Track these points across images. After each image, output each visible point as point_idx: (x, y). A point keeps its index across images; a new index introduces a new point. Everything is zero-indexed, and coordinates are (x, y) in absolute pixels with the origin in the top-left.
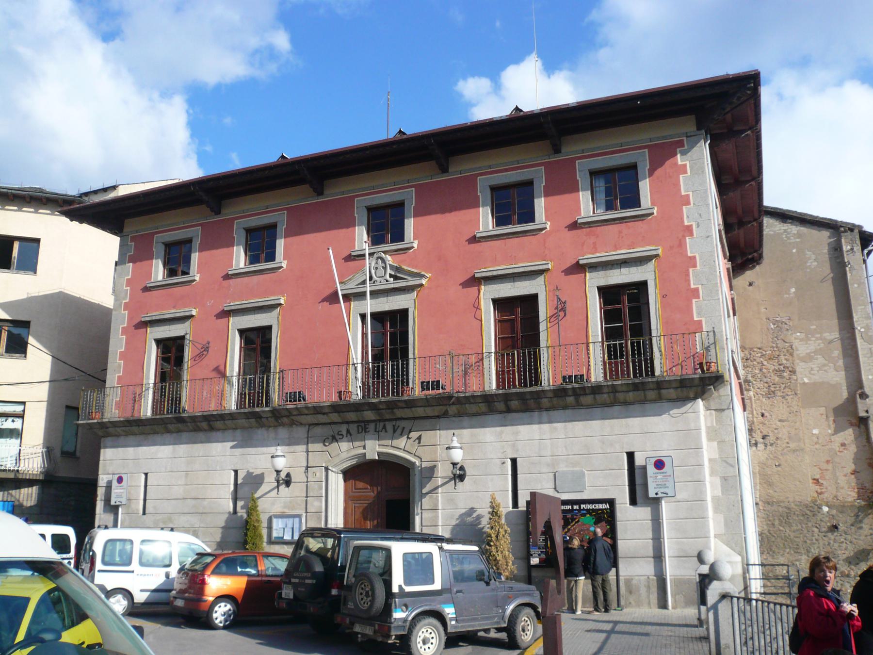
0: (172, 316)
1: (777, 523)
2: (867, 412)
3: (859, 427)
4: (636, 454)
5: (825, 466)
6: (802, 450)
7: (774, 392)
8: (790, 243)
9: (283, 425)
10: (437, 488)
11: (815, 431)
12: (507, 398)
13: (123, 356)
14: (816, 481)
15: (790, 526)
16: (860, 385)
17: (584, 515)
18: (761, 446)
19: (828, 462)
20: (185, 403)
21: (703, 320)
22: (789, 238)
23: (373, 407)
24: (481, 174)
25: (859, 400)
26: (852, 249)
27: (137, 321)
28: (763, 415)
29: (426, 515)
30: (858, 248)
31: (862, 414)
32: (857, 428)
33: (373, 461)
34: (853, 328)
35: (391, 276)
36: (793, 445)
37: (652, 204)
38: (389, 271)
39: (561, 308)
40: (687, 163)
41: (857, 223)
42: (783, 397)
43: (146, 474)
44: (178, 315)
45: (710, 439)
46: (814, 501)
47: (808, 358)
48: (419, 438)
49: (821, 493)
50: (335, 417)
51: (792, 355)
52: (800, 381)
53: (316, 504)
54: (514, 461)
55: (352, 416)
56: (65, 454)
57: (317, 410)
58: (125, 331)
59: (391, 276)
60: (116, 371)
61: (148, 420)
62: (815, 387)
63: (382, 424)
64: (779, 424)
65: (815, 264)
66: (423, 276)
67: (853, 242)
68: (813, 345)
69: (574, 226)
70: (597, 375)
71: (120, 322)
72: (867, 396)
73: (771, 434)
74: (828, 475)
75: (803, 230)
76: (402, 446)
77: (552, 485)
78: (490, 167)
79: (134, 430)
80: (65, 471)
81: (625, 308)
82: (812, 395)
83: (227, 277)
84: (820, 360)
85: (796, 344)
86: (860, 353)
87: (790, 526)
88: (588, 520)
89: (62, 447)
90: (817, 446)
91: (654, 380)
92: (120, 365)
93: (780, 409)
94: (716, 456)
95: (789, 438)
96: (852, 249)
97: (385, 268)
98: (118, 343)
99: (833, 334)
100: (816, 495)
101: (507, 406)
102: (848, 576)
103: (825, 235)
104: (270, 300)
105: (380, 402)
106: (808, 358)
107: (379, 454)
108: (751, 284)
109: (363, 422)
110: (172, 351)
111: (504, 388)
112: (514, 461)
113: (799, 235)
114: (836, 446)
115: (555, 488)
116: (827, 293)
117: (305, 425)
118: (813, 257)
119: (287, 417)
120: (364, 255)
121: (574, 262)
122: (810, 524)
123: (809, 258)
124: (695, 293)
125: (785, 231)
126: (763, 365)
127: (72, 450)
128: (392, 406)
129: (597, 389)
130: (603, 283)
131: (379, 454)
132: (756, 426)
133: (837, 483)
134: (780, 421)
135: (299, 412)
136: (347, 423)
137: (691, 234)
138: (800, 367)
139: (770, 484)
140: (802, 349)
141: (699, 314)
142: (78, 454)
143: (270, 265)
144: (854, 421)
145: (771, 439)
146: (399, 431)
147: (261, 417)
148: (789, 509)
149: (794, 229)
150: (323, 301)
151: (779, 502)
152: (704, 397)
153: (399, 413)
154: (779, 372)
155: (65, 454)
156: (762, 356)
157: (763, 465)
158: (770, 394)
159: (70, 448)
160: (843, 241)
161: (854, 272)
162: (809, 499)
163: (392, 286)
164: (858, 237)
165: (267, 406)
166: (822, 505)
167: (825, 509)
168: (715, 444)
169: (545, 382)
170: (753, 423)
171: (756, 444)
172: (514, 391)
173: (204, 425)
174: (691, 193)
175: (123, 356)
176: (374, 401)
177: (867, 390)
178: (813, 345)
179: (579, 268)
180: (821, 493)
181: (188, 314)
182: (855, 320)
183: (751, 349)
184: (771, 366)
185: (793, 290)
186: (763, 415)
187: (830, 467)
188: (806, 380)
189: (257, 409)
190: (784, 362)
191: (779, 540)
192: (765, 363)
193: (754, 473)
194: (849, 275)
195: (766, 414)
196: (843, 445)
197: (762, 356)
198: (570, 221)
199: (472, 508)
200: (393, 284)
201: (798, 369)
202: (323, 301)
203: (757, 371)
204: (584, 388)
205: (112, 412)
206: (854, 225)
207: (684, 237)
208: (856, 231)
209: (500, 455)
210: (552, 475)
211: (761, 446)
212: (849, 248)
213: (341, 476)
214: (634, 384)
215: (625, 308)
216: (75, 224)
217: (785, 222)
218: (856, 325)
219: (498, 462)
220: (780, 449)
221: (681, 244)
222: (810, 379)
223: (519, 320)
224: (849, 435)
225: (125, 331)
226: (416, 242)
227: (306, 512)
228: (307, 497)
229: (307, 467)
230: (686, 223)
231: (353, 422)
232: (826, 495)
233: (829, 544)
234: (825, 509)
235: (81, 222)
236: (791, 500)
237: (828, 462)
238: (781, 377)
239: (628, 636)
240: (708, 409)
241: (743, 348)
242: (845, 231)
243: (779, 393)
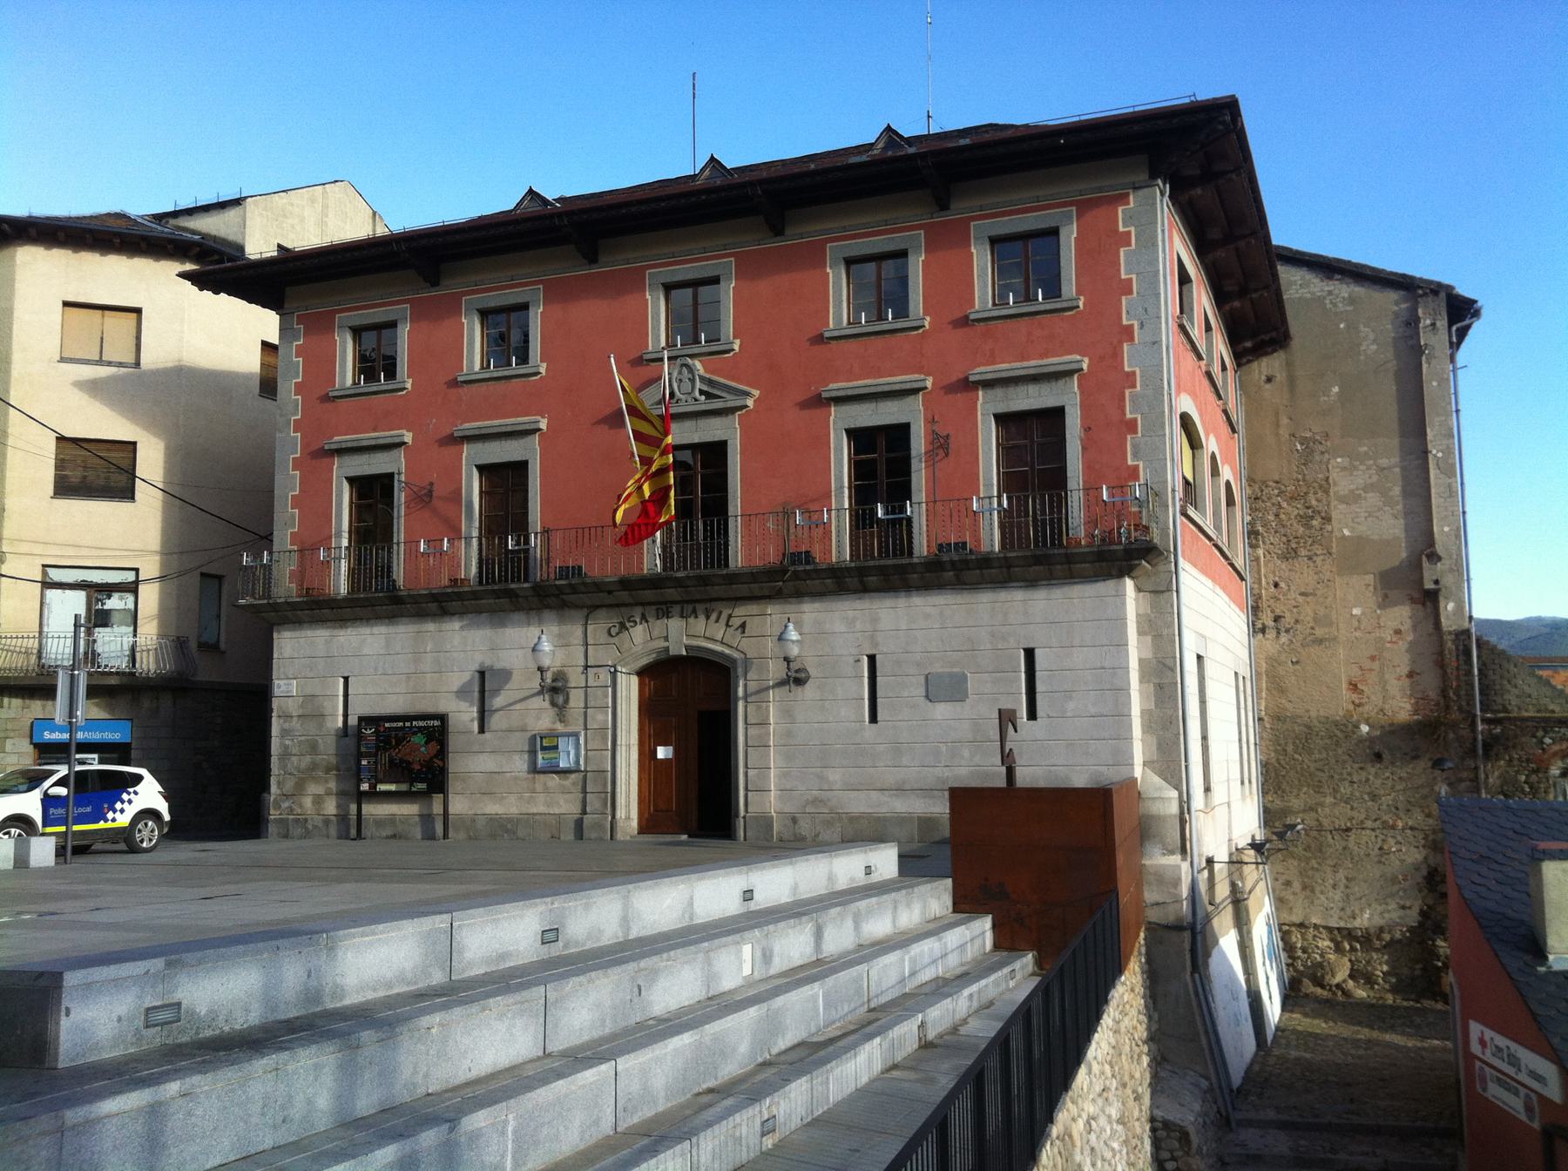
0: (373, 443)
1: (1290, 748)
2: (1437, 582)
3: (1424, 604)
4: (1037, 652)
5: (1367, 664)
6: (1335, 639)
7: (1295, 551)
8: (1336, 314)
9: (549, 607)
10: (768, 689)
11: (1356, 611)
12: (861, 572)
13: (297, 502)
14: (1354, 687)
15: (1310, 753)
16: (1431, 542)
17: (415, 733)
18: (1271, 634)
19: (1373, 658)
20: (399, 574)
21: (1141, 464)
22: (1335, 305)
23: (679, 583)
24: (468, 293)
25: (1425, 564)
26: (1433, 324)
27: (315, 446)
28: (1276, 585)
29: (752, 731)
30: (1442, 323)
31: (1429, 585)
32: (1420, 607)
33: (678, 659)
34: (1426, 452)
35: (702, 392)
36: (1319, 632)
37: (1079, 292)
38: (698, 385)
39: (940, 445)
40: (1133, 229)
41: (1446, 281)
42: (1310, 558)
43: (346, 679)
44: (381, 442)
45: (1140, 633)
46: (1349, 714)
47: (1352, 498)
48: (743, 626)
49: (1359, 705)
50: (624, 596)
51: (1327, 492)
52: (1336, 533)
53: (600, 717)
54: (872, 659)
55: (649, 595)
56: (204, 647)
57: (598, 587)
58: (297, 464)
59: (702, 392)
60: (287, 527)
61: (345, 599)
62: (1360, 542)
63: (690, 607)
64: (1300, 599)
65: (1374, 347)
66: (748, 394)
67: (1435, 314)
68: (1361, 478)
69: (964, 322)
70: (992, 538)
71: (291, 445)
72: (1439, 559)
73: (1287, 615)
74: (1373, 678)
75: (1359, 290)
76: (719, 637)
77: (922, 691)
78: (845, 229)
79: (317, 609)
80: (207, 672)
81: (1034, 442)
82: (1353, 556)
83: (454, 383)
84: (1373, 499)
85: (1334, 475)
86: (1433, 491)
87: (1310, 753)
88: (419, 739)
89: (199, 637)
90: (1358, 634)
91: (1062, 551)
92: (293, 516)
93: (1303, 575)
94: (1148, 654)
95: (1315, 619)
96: (1433, 324)
97: (692, 381)
98: (289, 483)
99: (1391, 460)
100: (1351, 707)
101: (861, 582)
102: (1393, 827)
103: (1390, 300)
104: (523, 421)
105: (688, 577)
106: (1352, 498)
107: (687, 648)
108: (1269, 380)
109: (666, 603)
110: (373, 494)
111: (685, 568)
112: (872, 659)
113: (1351, 300)
114: (1388, 635)
115: (927, 697)
116: (1386, 392)
117: (582, 607)
118: (1372, 336)
119: (557, 596)
120: (661, 360)
121: (961, 376)
122: (1340, 751)
123: (1365, 338)
124: (1132, 426)
125: (1330, 293)
126: (1280, 507)
127: (212, 641)
128: (704, 581)
129: (986, 561)
130: (1002, 408)
131: (687, 648)
132: (1264, 604)
133: (1385, 689)
134: (1302, 594)
135: (574, 589)
136: (642, 604)
137: (1132, 339)
138: (1338, 511)
139: (1282, 691)
140: (1343, 484)
141: (1135, 456)
142: (223, 646)
143: (523, 370)
144: (1416, 595)
145: (1288, 620)
146: (714, 616)
147: (517, 596)
148: (1309, 727)
149: (1344, 290)
150: (599, 422)
151: (1294, 719)
152: (1134, 574)
153: (715, 591)
154: (1305, 520)
155: (204, 647)
156: (1281, 493)
157: (1273, 662)
158: (1290, 554)
159: (209, 637)
160: (1420, 311)
161: (1434, 362)
162: (1341, 713)
163: (703, 407)
164: (1444, 304)
165: (526, 580)
166: (1359, 722)
167: (1365, 728)
168: (1149, 638)
169: (916, 552)
170: (1260, 597)
171: (1263, 630)
172: (872, 563)
173: (433, 606)
174: (1134, 277)
175: (297, 502)
176: (680, 574)
177: (1439, 549)
178: (1361, 478)
179: (968, 386)
180: (1359, 705)
181: (397, 440)
182: (1429, 437)
183: (1264, 482)
184: (1292, 510)
185: (1336, 389)
186: (1276, 585)
187: (1376, 665)
188: (1346, 532)
189: (513, 586)
190: (1314, 503)
191: (1292, 773)
192: (1284, 505)
193: (1258, 674)
194: (1425, 366)
195: (1282, 585)
196: (1398, 632)
197: (1281, 493)
198: (958, 315)
199: (627, 544)
200: (704, 404)
201: (1334, 515)
202: (599, 422)
203: (1271, 517)
204: (966, 562)
205: (286, 587)
206: (1439, 285)
207: (1121, 343)
208: (1443, 295)
209: (854, 651)
210: (922, 679)
211: (1271, 634)
212: (1428, 322)
213: (635, 680)
214: (1034, 556)
215: (1034, 442)
216: (207, 295)
217: (1330, 278)
218: (1430, 447)
219: (851, 660)
220: (1300, 637)
221: (1117, 355)
222: (1352, 530)
223: (882, 461)
224: (1401, 615)
225: (297, 464)
226: (738, 342)
227: (586, 729)
228: (586, 707)
229: (586, 667)
230: (1125, 322)
231: (650, 604)
232: (1367, 707)
233: (1367, 780)
234: (1365, 728)
235: (216, 292)
236: (1313, 714)
237: (1373, 658)
238: (1308, 526)
239: (204, 200)
240: (1139, 589)
241: (1251, 481)
242: (1425, 294)
243: (1303, 552)
